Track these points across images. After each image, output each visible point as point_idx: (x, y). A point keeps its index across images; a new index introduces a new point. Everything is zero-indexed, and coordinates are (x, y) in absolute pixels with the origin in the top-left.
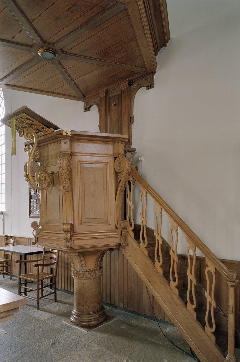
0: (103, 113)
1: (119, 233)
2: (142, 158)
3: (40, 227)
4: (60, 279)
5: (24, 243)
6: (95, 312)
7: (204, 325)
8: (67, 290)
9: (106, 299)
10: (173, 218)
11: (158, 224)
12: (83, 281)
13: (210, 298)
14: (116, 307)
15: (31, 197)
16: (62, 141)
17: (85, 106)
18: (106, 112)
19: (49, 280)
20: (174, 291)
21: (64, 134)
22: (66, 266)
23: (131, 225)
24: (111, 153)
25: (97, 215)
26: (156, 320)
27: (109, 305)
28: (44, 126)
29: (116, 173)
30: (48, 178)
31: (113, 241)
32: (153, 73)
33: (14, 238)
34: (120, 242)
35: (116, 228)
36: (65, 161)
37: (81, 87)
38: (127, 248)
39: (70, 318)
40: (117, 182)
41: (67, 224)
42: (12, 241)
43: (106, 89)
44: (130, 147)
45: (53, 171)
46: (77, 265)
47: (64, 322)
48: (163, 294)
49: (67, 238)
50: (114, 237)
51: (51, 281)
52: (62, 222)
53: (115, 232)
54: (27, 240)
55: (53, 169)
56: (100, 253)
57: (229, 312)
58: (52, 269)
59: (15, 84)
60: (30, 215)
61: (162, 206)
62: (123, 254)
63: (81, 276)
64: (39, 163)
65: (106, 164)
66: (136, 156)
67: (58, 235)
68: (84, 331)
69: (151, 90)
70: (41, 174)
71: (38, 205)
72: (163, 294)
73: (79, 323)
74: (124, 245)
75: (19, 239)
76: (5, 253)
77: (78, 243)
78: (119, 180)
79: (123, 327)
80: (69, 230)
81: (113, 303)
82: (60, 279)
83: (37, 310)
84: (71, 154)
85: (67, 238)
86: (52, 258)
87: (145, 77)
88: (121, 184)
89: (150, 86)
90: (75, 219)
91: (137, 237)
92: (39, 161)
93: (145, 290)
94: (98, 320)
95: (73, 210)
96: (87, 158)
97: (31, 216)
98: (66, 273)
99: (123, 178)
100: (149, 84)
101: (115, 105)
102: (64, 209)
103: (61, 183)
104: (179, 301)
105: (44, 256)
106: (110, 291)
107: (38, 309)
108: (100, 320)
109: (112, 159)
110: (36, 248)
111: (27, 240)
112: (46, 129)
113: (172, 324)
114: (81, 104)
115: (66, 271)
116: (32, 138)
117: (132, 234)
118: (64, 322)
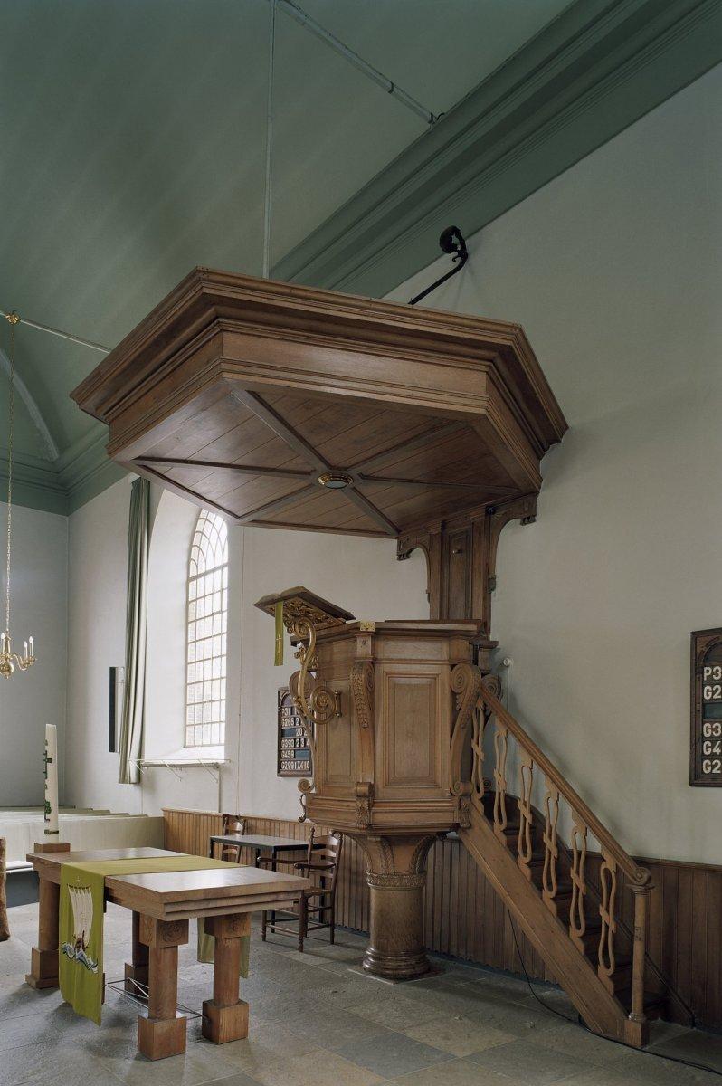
0: (436, 566)
1: (456, 803)
2: (510, 661)
3: (313, 791)
4: (340, 904)
5: (265, 830)
6: (407, 953)
7: (595, 963)
8: (353, 926)
9: (433, 941)
10: (551, 778)
11: (534, 791)
12: (388, 892)
13: (607, 917)
14: (452, 957)
15: (282, 733)
16: (358, 641)
17: (399, 549)
18: (441, 565)
19: (318, 898)
20: (550, 907)
21: (363, 629)
22: (354, 877)
23: (478, 790)
24: (445, 657)
25: (412, 762)
26: (528, 979)
27: (437, 953)
28: (329, 616)
29: (454, 694)
30: (331, 703)
31: (446, 819)
32: (535, 493)
33: (245, 820)
34: (457, 821)
35: (452, 795)
36: (363, 676)
37: (393, 518)
38: (469, 831)
39: (361, 965)
40: (455, 711)
41: (364, 783)
42: (239, 826)
43: (442, 519)
44: (488, 638)
45: (339, 689)
46: (375, 864)
47: (350, 970)
48: (533, 917)
49: (362, 808)
50: (446, 811)
51: (322, 902)
52: (354, 780)
53: (449, 802)
54: (272, 824)
55: (339, 685)
56: (423, 840)
57: (635, 938)
58: (323, 879)
59: (271, 520)
60: (279, 771)
61: (532, 755)
62: (468, 852)
63: (384, 884)
64: (314, 674)
65: (435, 677)
66: (498, 656)
67: (349, 803)
68: (390, 983)
69: (531, 527)
70: (321, 695)
71: (292, 751)
72: (533, 917)
73: (379, 971)
74: (465, 825)
75: (254, 822)
76: (225, 851)
77: (384, 817)
78: (458, 707)
79: (461, 984)
80: (367, 793)
81: (445, 950)
82: (340, 904)
83: (298, 952)
84: (374, 661)
85: (362, 808)
86: (323, 857)
87: (520, 501)
88: (460, 714)
89: (529, 518)
90: (378, 775)
91: (489, 815)
92: (319, 669)
93: (508, 922)
94: (414, 968)
95: (375, 761)
96: (402, 668)
97: (282, 772)
98: (354, 891)
99: (464, 705)
100: (526, 515)
101: (459, 551)
102: (359, 757)
103: (355, 712)
104: (556, 925)
105: (311, 854)
106: (441, 930)
107: (302, 951)
108: (418, 970)
109: (446, 669)
110: (292, 840)
111: (272, 824)
112: (331, 619)
113: (558, 986)
114: (393, 544)
115: (354, 887)
116: (308, 634)
117: (481, 807)
118: (350, 970)
